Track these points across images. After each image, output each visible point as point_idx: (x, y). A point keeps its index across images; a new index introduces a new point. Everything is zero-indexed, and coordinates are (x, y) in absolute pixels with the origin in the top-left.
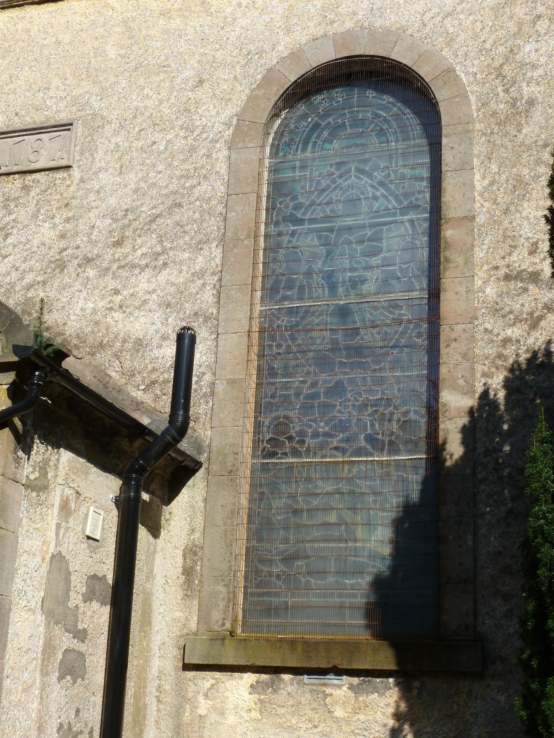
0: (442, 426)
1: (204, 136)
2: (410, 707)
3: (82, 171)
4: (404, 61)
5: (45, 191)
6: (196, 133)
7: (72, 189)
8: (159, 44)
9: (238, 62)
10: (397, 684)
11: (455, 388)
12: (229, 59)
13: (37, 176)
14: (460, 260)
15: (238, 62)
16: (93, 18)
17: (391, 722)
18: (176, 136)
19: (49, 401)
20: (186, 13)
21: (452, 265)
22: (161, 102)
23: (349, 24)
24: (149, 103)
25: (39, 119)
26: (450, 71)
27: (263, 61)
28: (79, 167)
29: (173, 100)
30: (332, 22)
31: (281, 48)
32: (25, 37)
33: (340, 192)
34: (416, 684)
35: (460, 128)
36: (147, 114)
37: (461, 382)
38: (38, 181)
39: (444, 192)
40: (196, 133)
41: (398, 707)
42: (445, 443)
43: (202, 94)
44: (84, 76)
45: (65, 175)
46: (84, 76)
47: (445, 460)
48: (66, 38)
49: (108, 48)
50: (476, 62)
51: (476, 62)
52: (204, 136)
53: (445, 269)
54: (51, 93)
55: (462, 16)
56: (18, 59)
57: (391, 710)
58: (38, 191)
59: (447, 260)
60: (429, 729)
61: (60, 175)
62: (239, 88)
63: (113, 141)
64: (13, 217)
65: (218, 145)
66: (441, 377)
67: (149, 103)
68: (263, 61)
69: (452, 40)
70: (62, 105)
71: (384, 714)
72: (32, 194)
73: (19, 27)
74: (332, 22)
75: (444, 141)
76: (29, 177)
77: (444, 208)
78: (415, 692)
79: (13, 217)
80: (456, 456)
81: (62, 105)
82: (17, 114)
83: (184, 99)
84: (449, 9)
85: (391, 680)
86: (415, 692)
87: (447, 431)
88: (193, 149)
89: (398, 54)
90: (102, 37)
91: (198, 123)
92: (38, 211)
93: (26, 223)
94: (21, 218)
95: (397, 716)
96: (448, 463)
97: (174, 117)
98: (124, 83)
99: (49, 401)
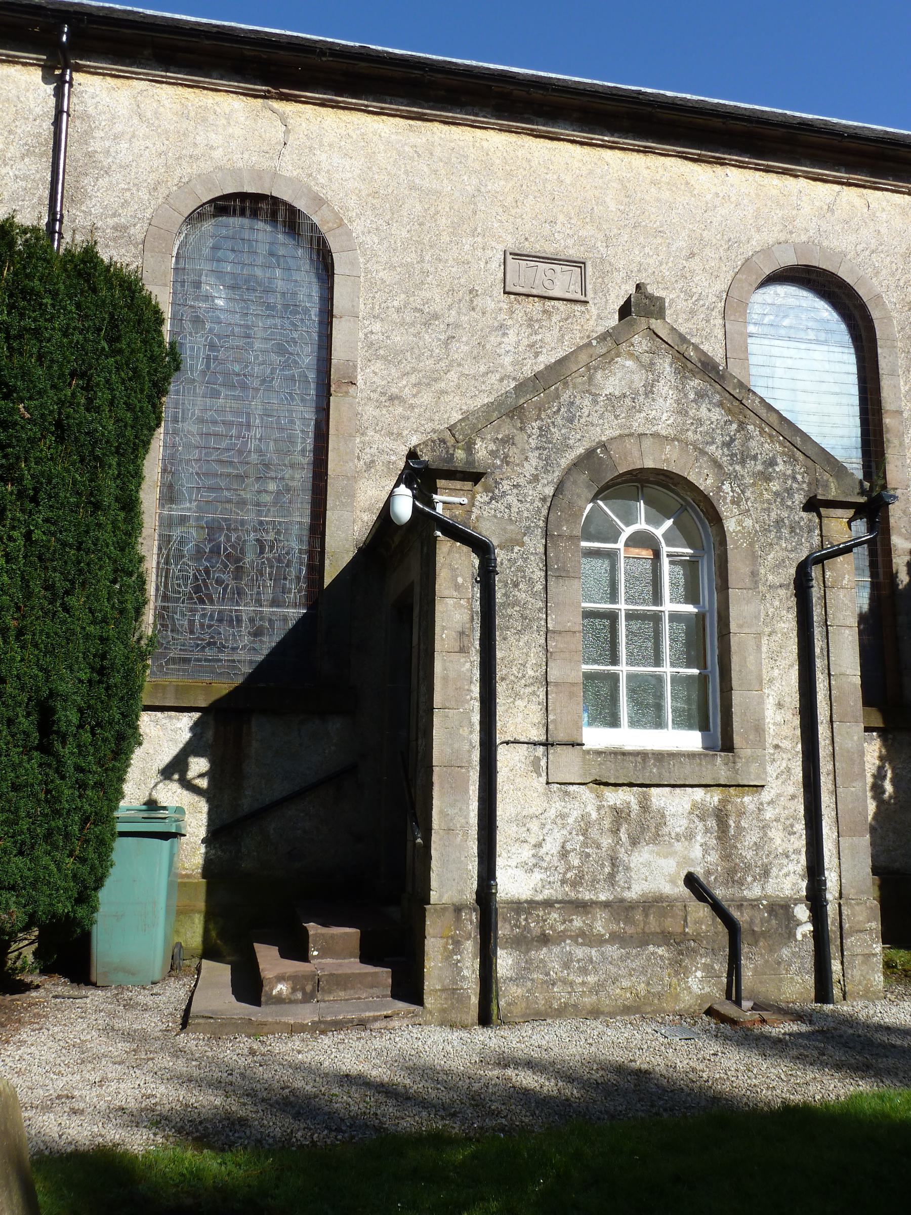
0: (894, 561)
1: (701, 302)
2: (887, 751)
3: (598, 309)
4: (848, 281)
5: (567, 319)
6: (694, 299)
7: (591, 323)
8: (654, 210)
9: (721, 246)
10: (879, 736)
11: (900, 534)
12: (714, 241)
13: (556, 303)
14: (896, 442)
15: (721, 246)
16: (590, 167)
17: (877, 762)
18: (678, 297)
19: (66, 30)
20: (674, 189)
21: (892, 445)
22: (661, 264)
23: (804, 238)
24: (651, 261)
25: (549, 249)
26: (879, 296)
27: (741, 250)
28: (595, 304)
29: (670, 264)
30: (791, 233)
31: (754, 243)
32: (525, 164)
33: (778, 362)
34: (890, 736)
35: (889, 343)
36: (650, 271)
37: (903, 530)
38: (558, 309)
39: (236, 173)
40: (694, 299)
41: (881, 751)
42: (897, 573)
43: (694, 264)
44: (588, 220)
45: (583, 309)
46: (588, 220)
47: (898, 585)
48: (568, 180)
49: (608, 200)
50: (895, 295)
51: (895, 295)
52: (701, 302)
53: (888, 448)
54: (558, 227)
55: (882, 255)
56: (522, 186)
57: (877, 754)
58: (558, 317)
59: (888, 441)
60: (900, 766)
61: (578, 307)
62: (724, 269)
63: (623, 287)
64: (539, 337)
65: (714, 313)
66: (891, 525)
67: (651, 261)
68: (741, 250)
69: (878, 272)
70: (570, 242)
71: (872, 756)
72: (554, 319)
73: (519, 153)
74: (791, 233)
75: (879, 350)
76: (548, 303)
77: (883, 402)
78: (890, 741)
79: (539, 337)
80: (905, 583)
81: (570, 242)
82: (526, 239)
83: (681, 267)
84: (873, 247)
85: (875, 734)
86: (890, 741)
87: (898, 565)
88: (693, 312)
89: (843, 274)
90: (601, 188)
91: (694, 290)
92: (563, 336)
93: (553, 345)
94: (548, 339)
95: (881, 758)
96: (901, 587)
97: (673, 280)
98: (626, 237)
99: (66, 30)
